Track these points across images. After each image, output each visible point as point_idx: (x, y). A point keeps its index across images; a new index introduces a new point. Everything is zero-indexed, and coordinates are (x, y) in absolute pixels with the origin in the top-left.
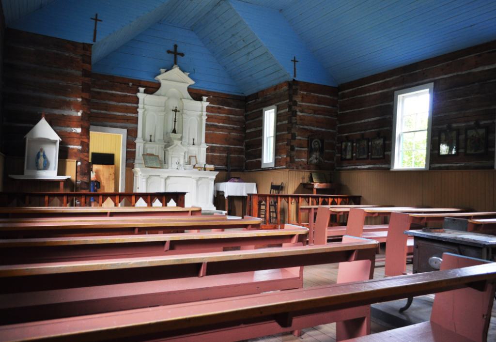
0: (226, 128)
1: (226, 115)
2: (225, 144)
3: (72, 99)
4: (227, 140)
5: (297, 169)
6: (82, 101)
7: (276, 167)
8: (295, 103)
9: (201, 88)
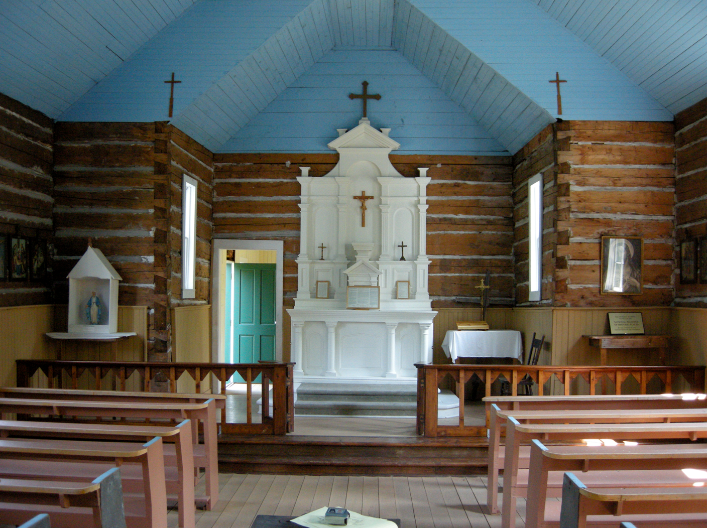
0: (473, 222)
1: (472, 198)
2: (470, 254)
3: (140, 211)
4: (473, 245)
5: (573, 305)
6: (154, 213)
7: (545, 302)
8: (565, 168)
9: (418, 153)
